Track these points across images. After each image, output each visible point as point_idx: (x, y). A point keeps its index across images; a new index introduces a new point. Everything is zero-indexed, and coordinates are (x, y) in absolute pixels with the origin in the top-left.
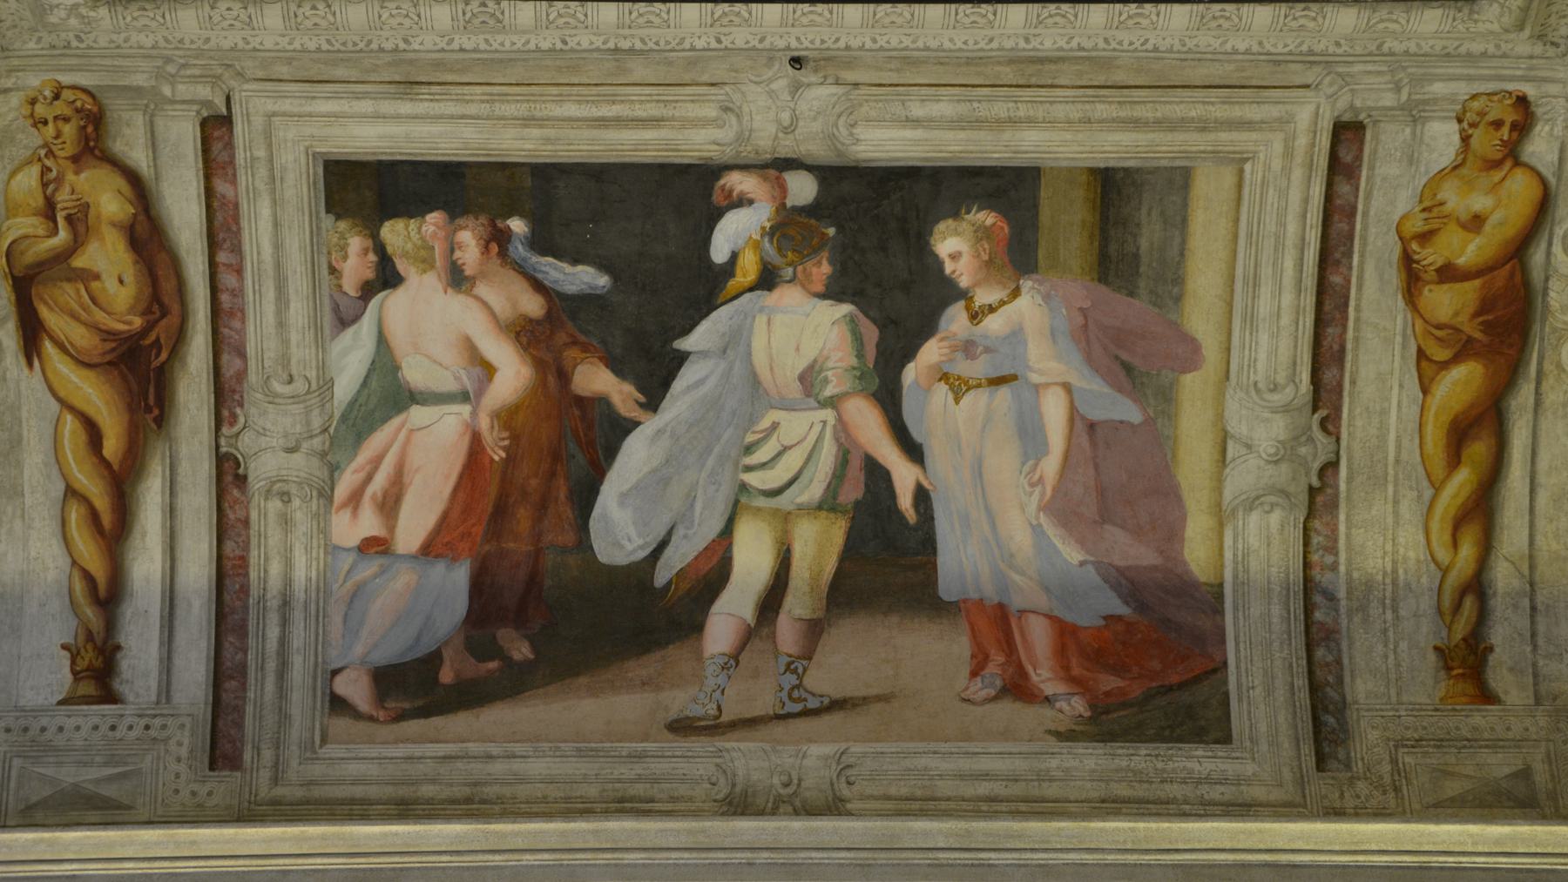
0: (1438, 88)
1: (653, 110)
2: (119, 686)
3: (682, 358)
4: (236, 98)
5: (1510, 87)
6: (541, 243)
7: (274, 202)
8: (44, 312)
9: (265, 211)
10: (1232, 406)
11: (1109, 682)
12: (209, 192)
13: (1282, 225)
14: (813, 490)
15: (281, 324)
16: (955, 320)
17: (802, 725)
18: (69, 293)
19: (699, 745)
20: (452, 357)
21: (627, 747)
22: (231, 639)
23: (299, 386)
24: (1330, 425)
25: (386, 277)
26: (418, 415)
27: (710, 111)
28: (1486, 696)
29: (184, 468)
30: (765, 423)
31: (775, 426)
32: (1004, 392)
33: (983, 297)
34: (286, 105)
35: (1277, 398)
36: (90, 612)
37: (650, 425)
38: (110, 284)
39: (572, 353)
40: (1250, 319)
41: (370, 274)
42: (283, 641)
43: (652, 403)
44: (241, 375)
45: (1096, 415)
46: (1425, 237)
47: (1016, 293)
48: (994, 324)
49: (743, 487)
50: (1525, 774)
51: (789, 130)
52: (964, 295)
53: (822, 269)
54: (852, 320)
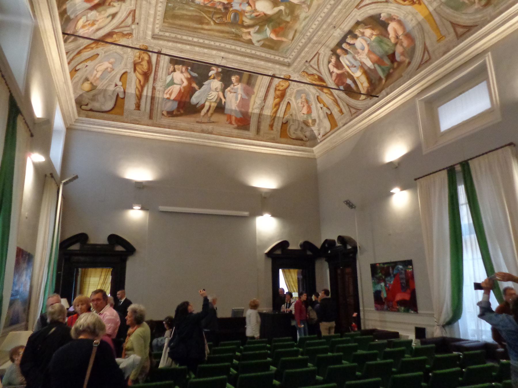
0: (283, 73)
2: (140, 109)
3: (203, 85)
4: (162, 49)
5: (290, 74)
6: (192, 70)
7: (164, 61)
8: (137, 68)
9: (163, 62)
11: (239, 124)
12: (157, 59)
14: (214, 100)
16: (232, 86)
17: (209, 124)
18: (140, 66)
19: (199, 124)
20: (180, 80)
21: (192, 123)
23: (163, 80)
24: (265, 102)
25: (174, 71)
26: (175, 86)
28: (272, 130)
32: (235, 94)
33: (235, 84)
35: (261, 99)
36: (138, 101)
37: (199, 91)
41: (173, 70)
42: (158, 107)
43: (200, 89)
45: (243, 97)
46: (278, 86)
47: (238, 84)
48: (236, 87)
49: (207, 99)
50: (274, 137)
51: (221, 63)
52: (233, 84)
53: (220, 78)
54: (221, 84)
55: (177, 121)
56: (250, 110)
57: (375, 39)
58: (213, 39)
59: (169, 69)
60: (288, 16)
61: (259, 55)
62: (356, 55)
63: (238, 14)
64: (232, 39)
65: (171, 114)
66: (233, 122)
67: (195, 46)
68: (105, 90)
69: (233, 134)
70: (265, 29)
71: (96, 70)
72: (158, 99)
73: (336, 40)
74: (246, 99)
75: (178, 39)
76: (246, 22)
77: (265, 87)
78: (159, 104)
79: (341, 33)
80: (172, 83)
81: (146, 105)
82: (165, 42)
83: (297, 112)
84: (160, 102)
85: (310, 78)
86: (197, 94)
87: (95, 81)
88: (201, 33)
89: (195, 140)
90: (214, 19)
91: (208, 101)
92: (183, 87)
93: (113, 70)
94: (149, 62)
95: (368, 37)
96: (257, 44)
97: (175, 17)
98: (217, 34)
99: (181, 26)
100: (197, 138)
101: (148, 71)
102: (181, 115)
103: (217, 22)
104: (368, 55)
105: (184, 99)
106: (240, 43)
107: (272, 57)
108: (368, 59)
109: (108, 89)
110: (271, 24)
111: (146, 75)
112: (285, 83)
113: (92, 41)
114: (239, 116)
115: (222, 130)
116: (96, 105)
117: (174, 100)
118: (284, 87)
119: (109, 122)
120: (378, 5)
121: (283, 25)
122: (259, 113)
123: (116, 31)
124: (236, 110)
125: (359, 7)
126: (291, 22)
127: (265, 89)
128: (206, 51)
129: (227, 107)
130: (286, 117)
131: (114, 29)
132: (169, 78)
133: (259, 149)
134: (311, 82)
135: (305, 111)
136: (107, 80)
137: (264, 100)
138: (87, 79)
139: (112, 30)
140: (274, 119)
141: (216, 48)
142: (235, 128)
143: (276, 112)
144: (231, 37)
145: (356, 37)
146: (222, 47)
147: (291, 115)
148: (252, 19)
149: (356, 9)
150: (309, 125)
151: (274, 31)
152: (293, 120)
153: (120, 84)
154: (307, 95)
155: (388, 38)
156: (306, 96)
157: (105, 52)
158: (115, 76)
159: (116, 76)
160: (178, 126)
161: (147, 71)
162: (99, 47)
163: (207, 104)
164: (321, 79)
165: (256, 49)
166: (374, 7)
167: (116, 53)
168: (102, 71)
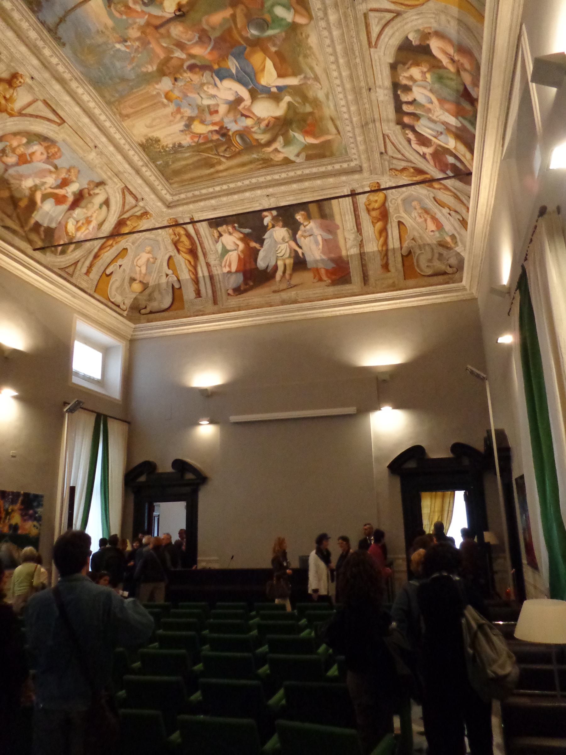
1: (249, 206)
2: (202, 296)
6: (240, 227)
8: (179, 248)
10: (346, 233)
11: (334, 277)
13: (347, 207)
15: (209, 244)
16: (302, 228)
17: (291, 289)
21: (267, 296)
22: (214, 287)
23: (214, 252)
24: (361, 234)
25: (221, 235)
26: (230, 253)
27: (258, 205)
28: (389, 271)
29: (202, 265)
30: (278, 247)
31: (280, 247)
32: (312, 237)
34: (199, 215)
36: (196, 286)
37: (262, 250)
38: (186, 243)
39: (248, 241)
40: (346, 221)
41: (218, 235)
43: (262, 246)
44: (206, 252)
46: (369, 205)
47: (310, 222)
48: (308, 227)
49: (277, 256)
50: (394, 283)
51: (270, 205)
52: (302, 224)
54: (287, 230)
55: (247, 298)
56: (344, 253)
57: (431, 76)
58: (239, 179)
59: (214, 236)
60: (304, 104)
61: (309, 174)
62: (430, 115)
63: (243, 134)
64: (263, 168)
65: (238, 291)
66: (324, 278)
67: (220, 196)
68: (158, 285)
69: (326, 294)
70: (293, 135)
71: (137, 265)
72: (217, 277)
73: (389, 106)
74: (329, 239)
75: (198, 196)
76: (262, 139)
77: (349, 212)
78: (221, 283)
79: (386, 92)
80: (225, 251)
81: (206, 288)
82: (184, 206)
83: (421, 231)
84: (221, 280)
85: (405, 175)
86: (261, 254)
87: (144, 278)
88: (220, 177)
89: (273, 318)
90: (222, 154)
91: (280, 259)
92: (241, 252)
93: (156, 259)
94: (188, 235)
95: (422, 80)
96: (298, 160)
97: (177, 173)
98: (239, 170)
99: (192, 179)
100: (274, 314)
101: (192, 247)
102: (251, 288)
103: (228, 156)
104: (442, 107)
105: (248, 267)
106: (277, 169)
107: (330, 168)
108: (447, 114)
109: (160, 282)
110: (294, 126)
111: (193, 252)
112: (377, 196)
113: (104, 240)
114: (331, 265)
115: (310, 293)
116: (155, 305)
117: (237, 271)
118: (378, 201)
119: (157, 323)
120: (393, 27)
121: (310, 120)
122: (358, 252)
123: (125, 216)
124: (322, 260)
125: (373, 44)
126: (316, 111)
127: (352, 215)
128: (236, 197)
129: (308, 259)
130: (405, 245)
131: (120, 216)
132: (219, 247)
133: (370, 307)
134: (412, 180)
135: (431, 226)
136: (156, 272)
137: (358, 232)
138: (133, 280)
139: (119, 217)
140: (386, 255)
141: (248, 188)
142: (328, 286)
143: (386, 243)
144: (260, 166)
145: (407, 89)
146: (255, 183)
147: (413, 239)
148: (265, 132)
149: (372, 50)
150: (449, 246)
151: (307, 133)
152: (419, 245)
153: (170, 272)
154: (420, 201)
155: (445, 68)
156: (420, 203)
157: (133, 243)
158: (161, 265)
159: (162, 265)
160: (250, 304)
161: (191, 247)
162: (120, 241)
163: (280, 263)
164: (420, 171)
165: (301, 167)
166: (390, 33)
167: (147, 239)
168: (145, 265)
